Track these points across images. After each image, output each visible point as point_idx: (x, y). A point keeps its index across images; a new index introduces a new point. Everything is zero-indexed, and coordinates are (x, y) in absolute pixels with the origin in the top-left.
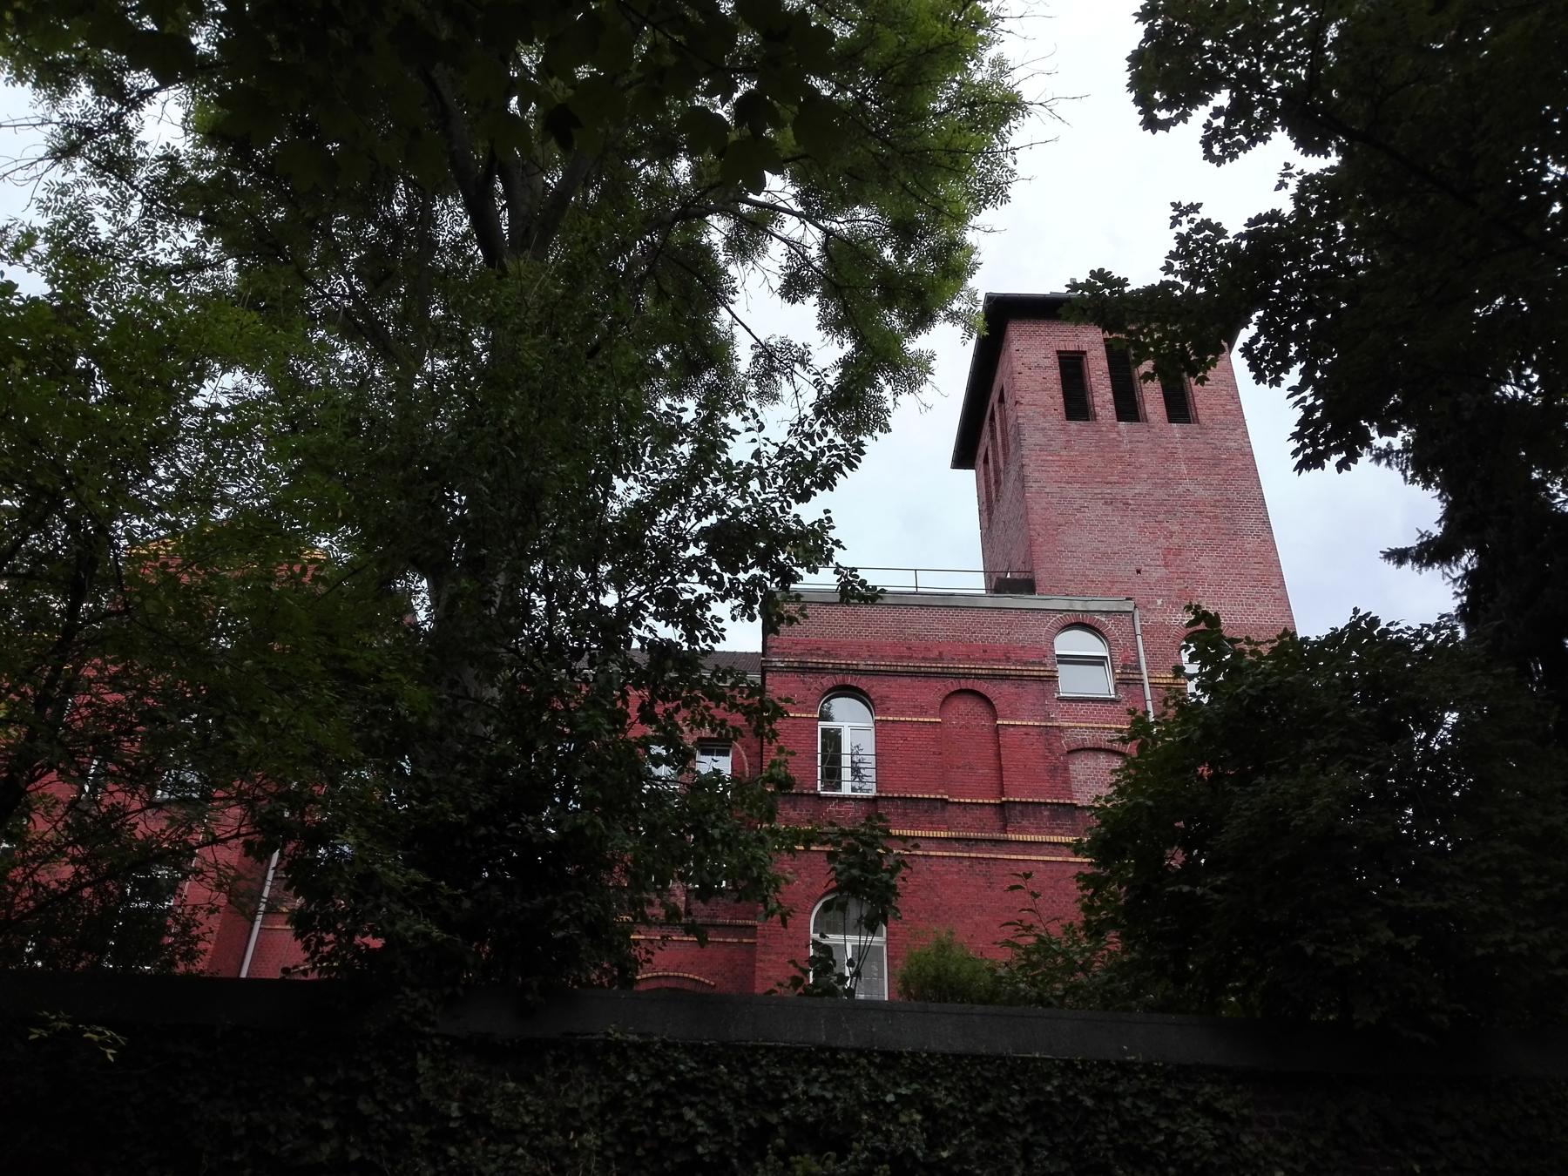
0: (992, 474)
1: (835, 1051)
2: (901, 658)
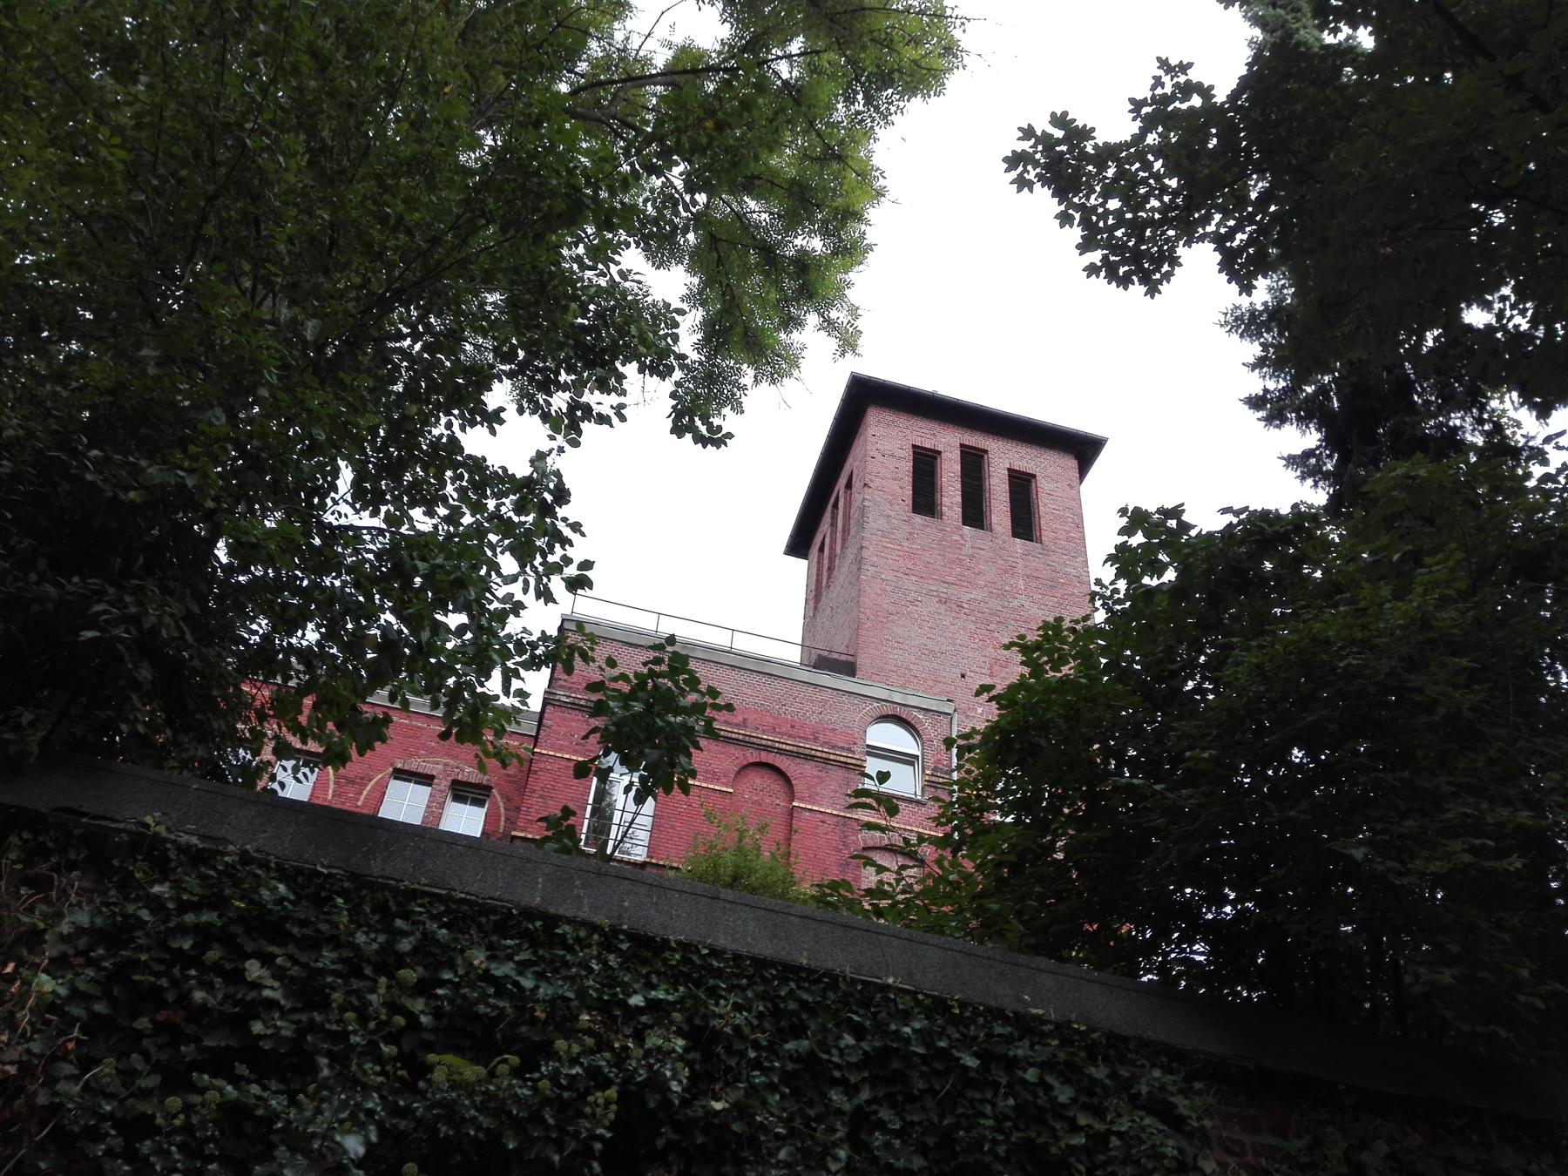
1: (552, 921)
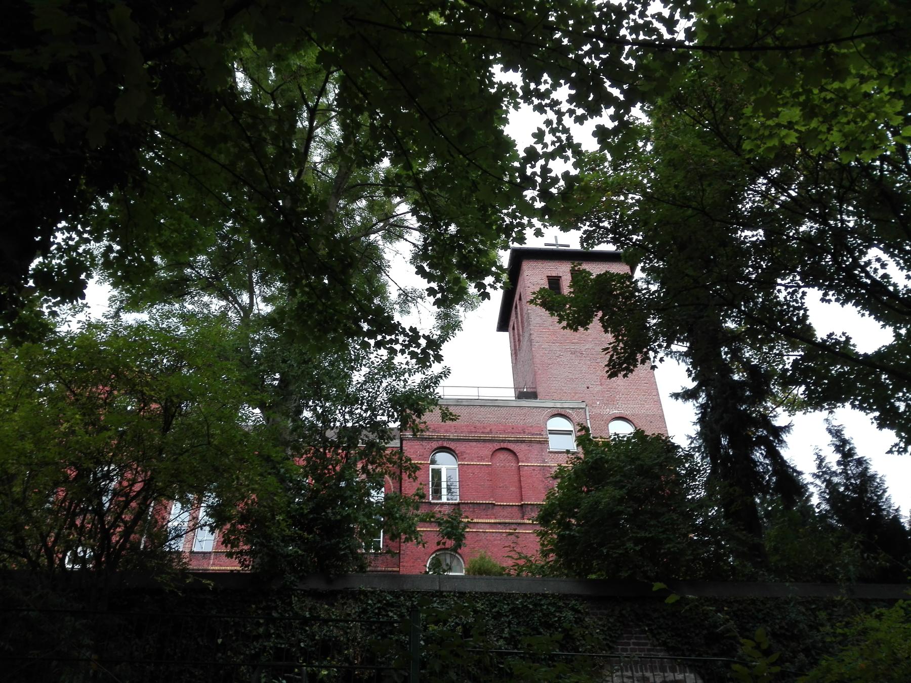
0: (517, 336)
1: (442, 592)
2: (471, 432)
